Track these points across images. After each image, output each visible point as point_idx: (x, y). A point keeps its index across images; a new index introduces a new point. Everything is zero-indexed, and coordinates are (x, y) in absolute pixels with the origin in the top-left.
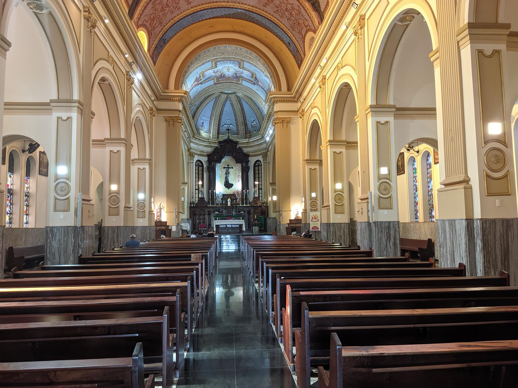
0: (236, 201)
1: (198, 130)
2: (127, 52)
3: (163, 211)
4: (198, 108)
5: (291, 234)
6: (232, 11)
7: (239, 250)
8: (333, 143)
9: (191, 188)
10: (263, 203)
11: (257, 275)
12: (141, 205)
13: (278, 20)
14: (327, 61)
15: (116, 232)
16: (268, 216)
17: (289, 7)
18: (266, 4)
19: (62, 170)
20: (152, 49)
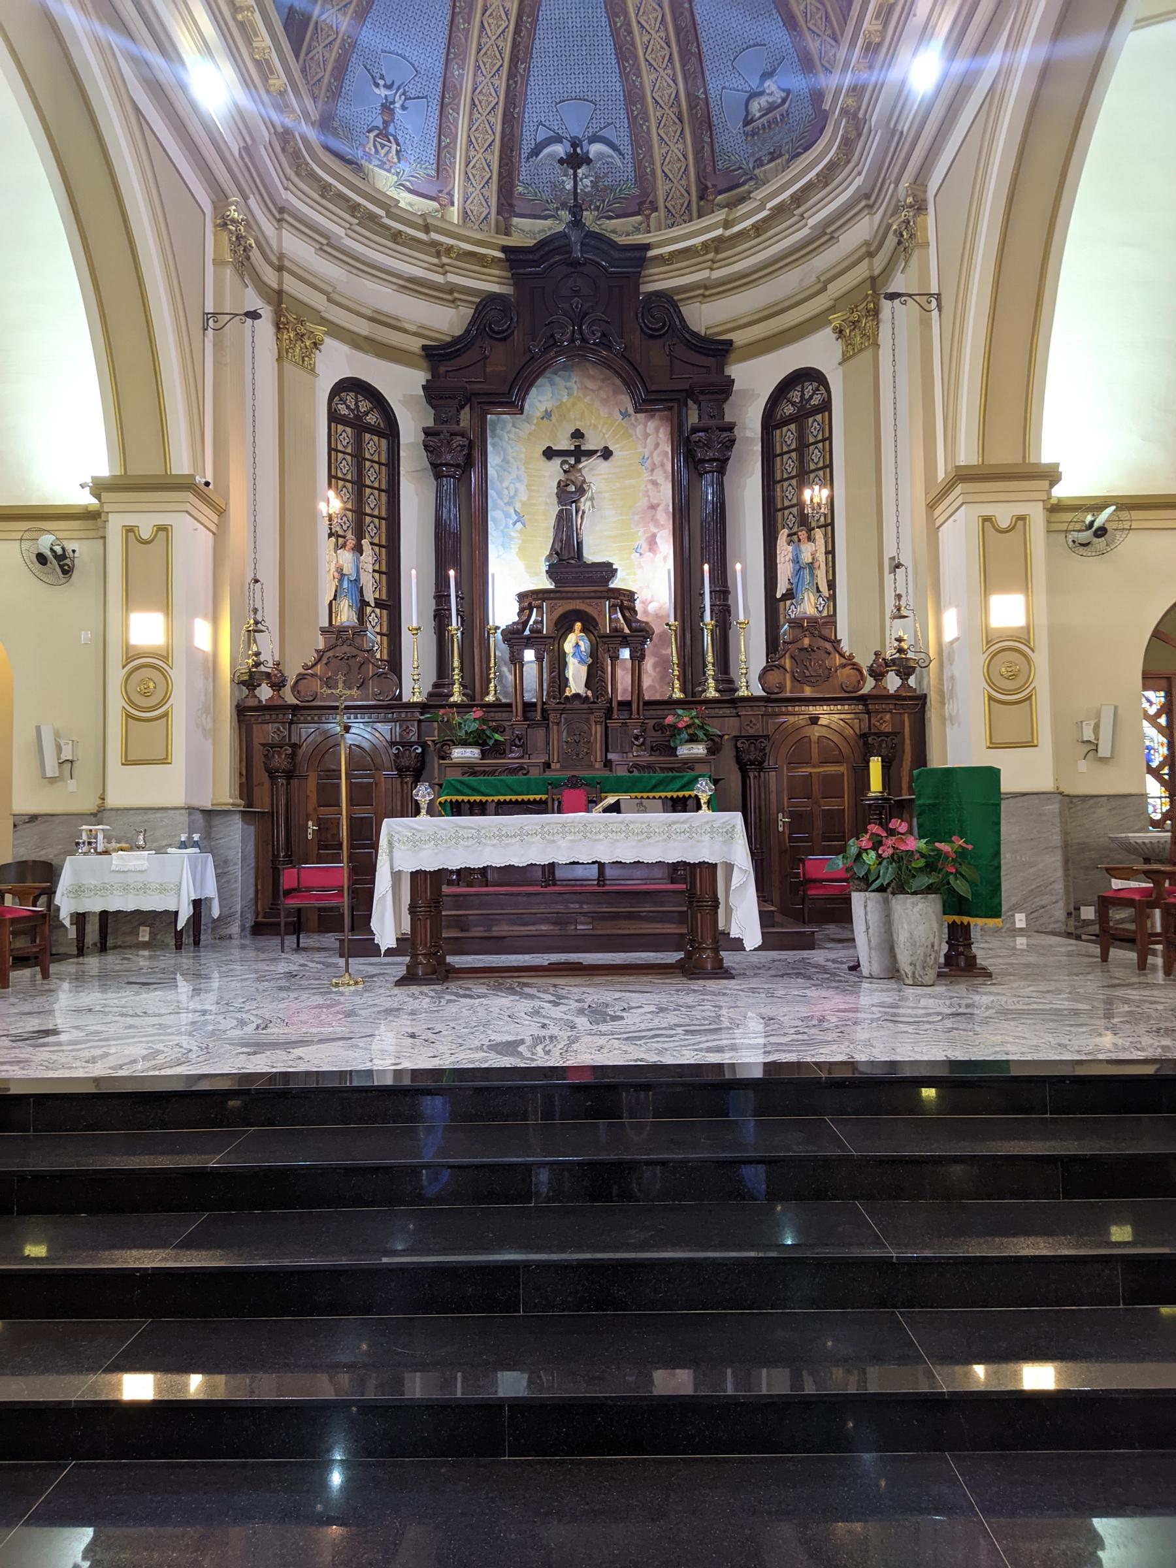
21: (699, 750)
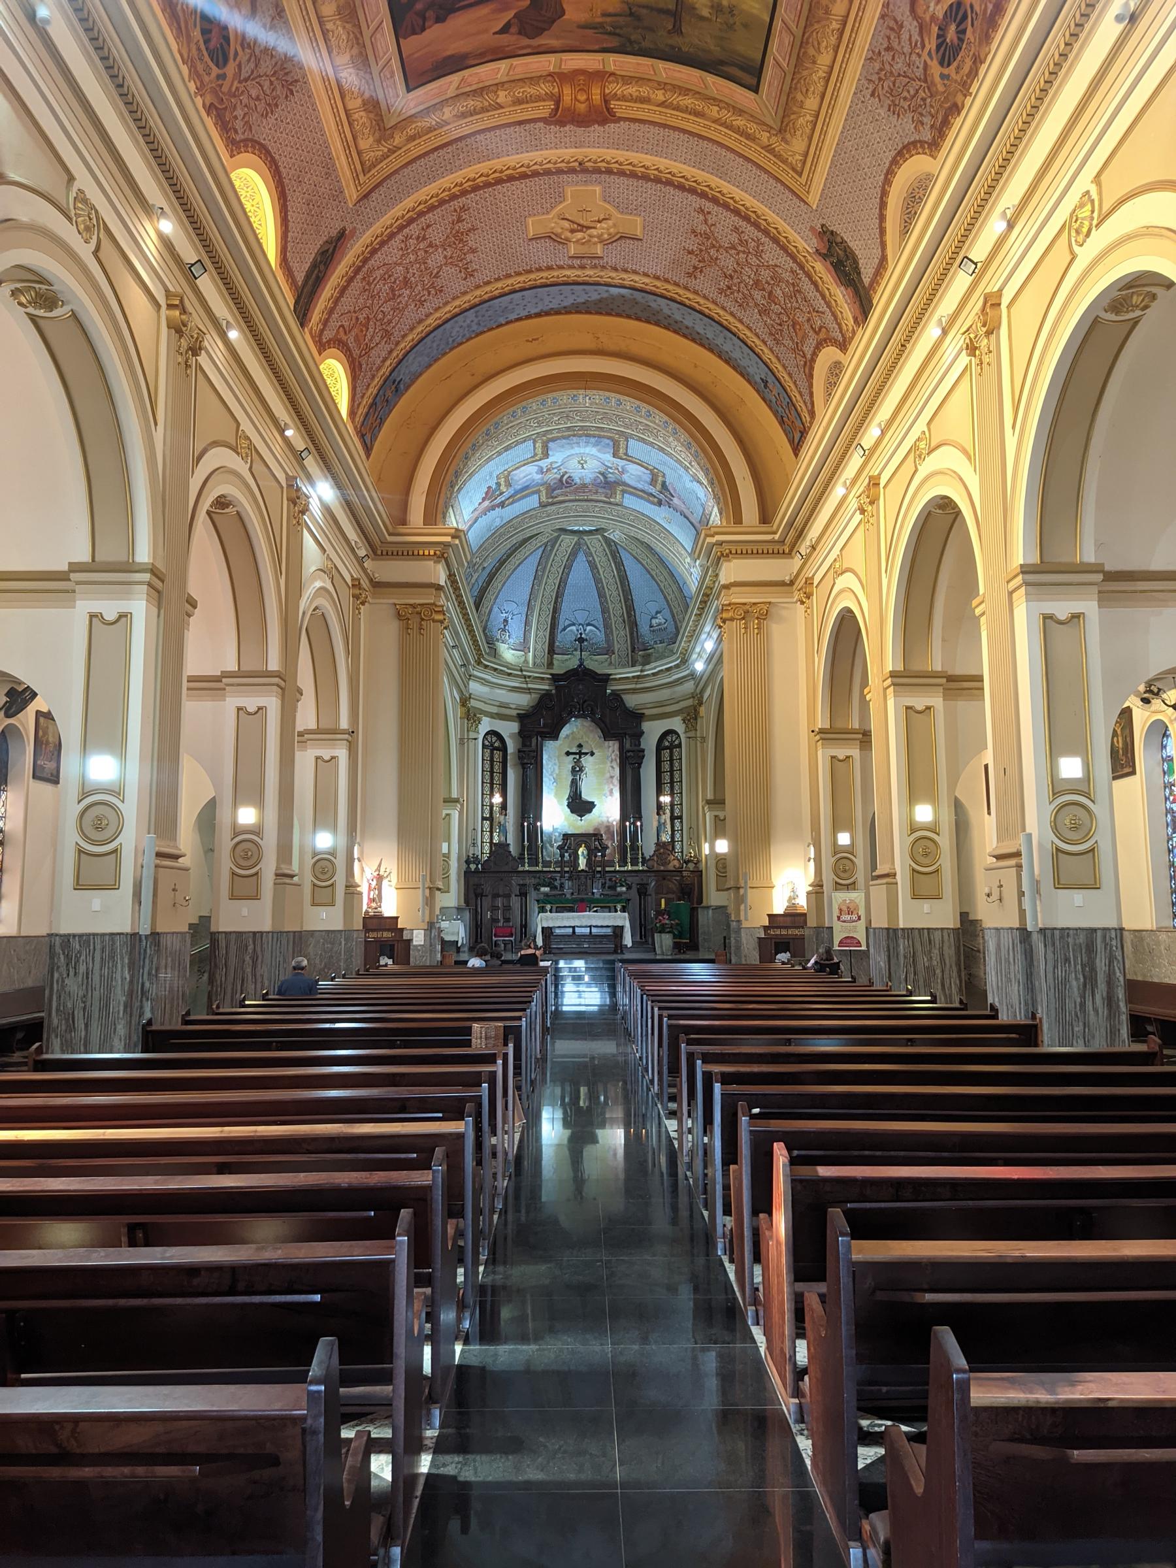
0: (603, 856)
1: (491, 642)
2: (288, 421)
3: (386, 884)
4: (491, 577)
5: (773, 960)
6: (594, 294)
7: (614, 1007)
8: (903, 679)
9: (468, 818)
10: (687, 862)
11: (674, 1090)
12: (323, 865)
13: (732, 314)
14: (883, 433)
15: (251, 947)
16: (700, 901)
17: (765, 274)
18: (695, 268)
19: (102, 768)
20: (362, 411)
21: (624, 889)
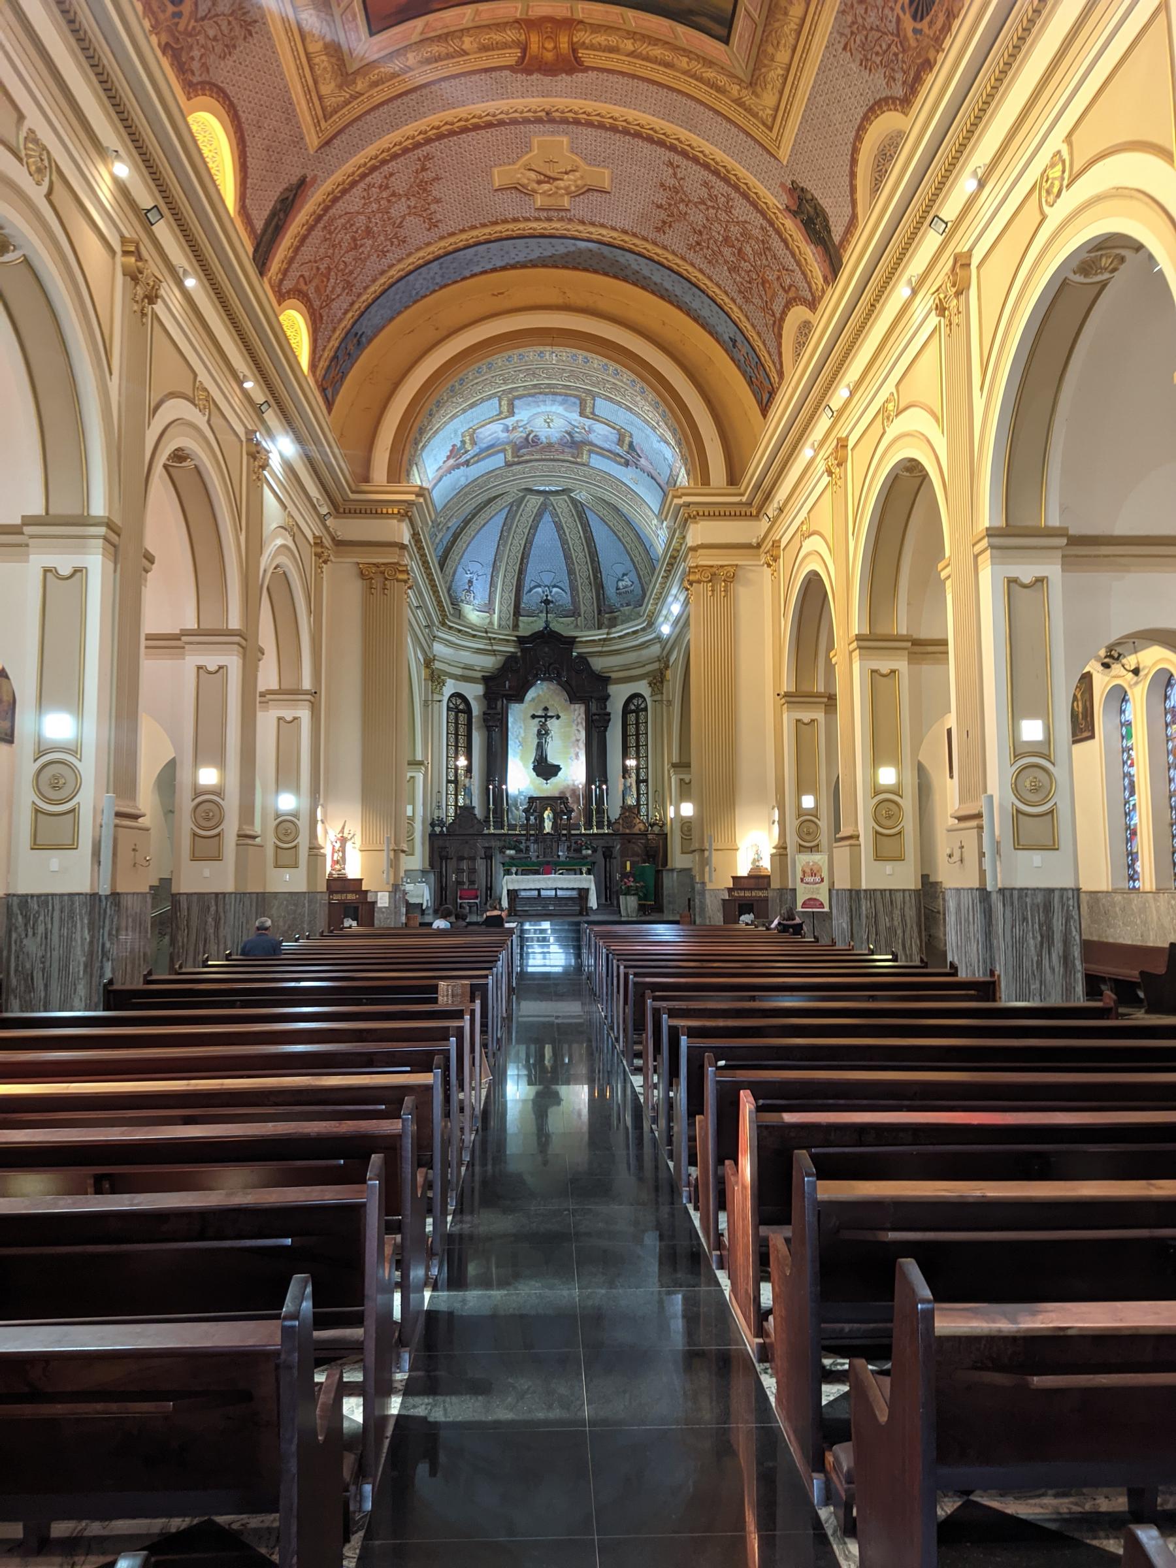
21: (590, 852)
